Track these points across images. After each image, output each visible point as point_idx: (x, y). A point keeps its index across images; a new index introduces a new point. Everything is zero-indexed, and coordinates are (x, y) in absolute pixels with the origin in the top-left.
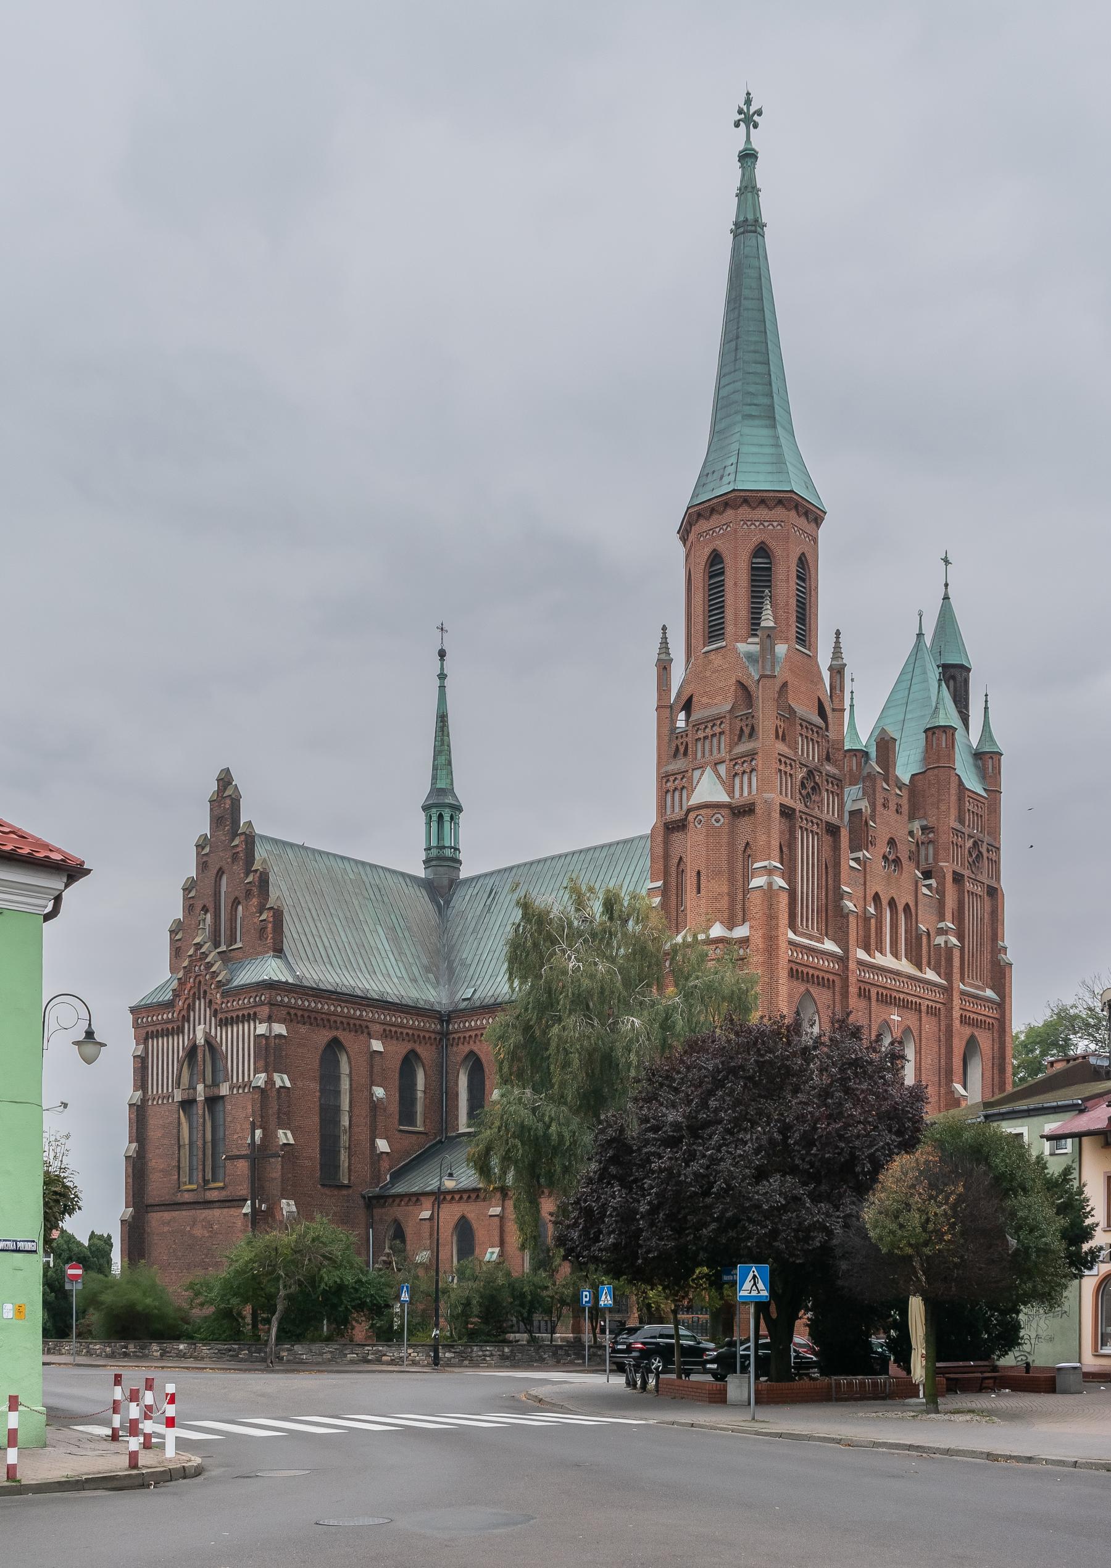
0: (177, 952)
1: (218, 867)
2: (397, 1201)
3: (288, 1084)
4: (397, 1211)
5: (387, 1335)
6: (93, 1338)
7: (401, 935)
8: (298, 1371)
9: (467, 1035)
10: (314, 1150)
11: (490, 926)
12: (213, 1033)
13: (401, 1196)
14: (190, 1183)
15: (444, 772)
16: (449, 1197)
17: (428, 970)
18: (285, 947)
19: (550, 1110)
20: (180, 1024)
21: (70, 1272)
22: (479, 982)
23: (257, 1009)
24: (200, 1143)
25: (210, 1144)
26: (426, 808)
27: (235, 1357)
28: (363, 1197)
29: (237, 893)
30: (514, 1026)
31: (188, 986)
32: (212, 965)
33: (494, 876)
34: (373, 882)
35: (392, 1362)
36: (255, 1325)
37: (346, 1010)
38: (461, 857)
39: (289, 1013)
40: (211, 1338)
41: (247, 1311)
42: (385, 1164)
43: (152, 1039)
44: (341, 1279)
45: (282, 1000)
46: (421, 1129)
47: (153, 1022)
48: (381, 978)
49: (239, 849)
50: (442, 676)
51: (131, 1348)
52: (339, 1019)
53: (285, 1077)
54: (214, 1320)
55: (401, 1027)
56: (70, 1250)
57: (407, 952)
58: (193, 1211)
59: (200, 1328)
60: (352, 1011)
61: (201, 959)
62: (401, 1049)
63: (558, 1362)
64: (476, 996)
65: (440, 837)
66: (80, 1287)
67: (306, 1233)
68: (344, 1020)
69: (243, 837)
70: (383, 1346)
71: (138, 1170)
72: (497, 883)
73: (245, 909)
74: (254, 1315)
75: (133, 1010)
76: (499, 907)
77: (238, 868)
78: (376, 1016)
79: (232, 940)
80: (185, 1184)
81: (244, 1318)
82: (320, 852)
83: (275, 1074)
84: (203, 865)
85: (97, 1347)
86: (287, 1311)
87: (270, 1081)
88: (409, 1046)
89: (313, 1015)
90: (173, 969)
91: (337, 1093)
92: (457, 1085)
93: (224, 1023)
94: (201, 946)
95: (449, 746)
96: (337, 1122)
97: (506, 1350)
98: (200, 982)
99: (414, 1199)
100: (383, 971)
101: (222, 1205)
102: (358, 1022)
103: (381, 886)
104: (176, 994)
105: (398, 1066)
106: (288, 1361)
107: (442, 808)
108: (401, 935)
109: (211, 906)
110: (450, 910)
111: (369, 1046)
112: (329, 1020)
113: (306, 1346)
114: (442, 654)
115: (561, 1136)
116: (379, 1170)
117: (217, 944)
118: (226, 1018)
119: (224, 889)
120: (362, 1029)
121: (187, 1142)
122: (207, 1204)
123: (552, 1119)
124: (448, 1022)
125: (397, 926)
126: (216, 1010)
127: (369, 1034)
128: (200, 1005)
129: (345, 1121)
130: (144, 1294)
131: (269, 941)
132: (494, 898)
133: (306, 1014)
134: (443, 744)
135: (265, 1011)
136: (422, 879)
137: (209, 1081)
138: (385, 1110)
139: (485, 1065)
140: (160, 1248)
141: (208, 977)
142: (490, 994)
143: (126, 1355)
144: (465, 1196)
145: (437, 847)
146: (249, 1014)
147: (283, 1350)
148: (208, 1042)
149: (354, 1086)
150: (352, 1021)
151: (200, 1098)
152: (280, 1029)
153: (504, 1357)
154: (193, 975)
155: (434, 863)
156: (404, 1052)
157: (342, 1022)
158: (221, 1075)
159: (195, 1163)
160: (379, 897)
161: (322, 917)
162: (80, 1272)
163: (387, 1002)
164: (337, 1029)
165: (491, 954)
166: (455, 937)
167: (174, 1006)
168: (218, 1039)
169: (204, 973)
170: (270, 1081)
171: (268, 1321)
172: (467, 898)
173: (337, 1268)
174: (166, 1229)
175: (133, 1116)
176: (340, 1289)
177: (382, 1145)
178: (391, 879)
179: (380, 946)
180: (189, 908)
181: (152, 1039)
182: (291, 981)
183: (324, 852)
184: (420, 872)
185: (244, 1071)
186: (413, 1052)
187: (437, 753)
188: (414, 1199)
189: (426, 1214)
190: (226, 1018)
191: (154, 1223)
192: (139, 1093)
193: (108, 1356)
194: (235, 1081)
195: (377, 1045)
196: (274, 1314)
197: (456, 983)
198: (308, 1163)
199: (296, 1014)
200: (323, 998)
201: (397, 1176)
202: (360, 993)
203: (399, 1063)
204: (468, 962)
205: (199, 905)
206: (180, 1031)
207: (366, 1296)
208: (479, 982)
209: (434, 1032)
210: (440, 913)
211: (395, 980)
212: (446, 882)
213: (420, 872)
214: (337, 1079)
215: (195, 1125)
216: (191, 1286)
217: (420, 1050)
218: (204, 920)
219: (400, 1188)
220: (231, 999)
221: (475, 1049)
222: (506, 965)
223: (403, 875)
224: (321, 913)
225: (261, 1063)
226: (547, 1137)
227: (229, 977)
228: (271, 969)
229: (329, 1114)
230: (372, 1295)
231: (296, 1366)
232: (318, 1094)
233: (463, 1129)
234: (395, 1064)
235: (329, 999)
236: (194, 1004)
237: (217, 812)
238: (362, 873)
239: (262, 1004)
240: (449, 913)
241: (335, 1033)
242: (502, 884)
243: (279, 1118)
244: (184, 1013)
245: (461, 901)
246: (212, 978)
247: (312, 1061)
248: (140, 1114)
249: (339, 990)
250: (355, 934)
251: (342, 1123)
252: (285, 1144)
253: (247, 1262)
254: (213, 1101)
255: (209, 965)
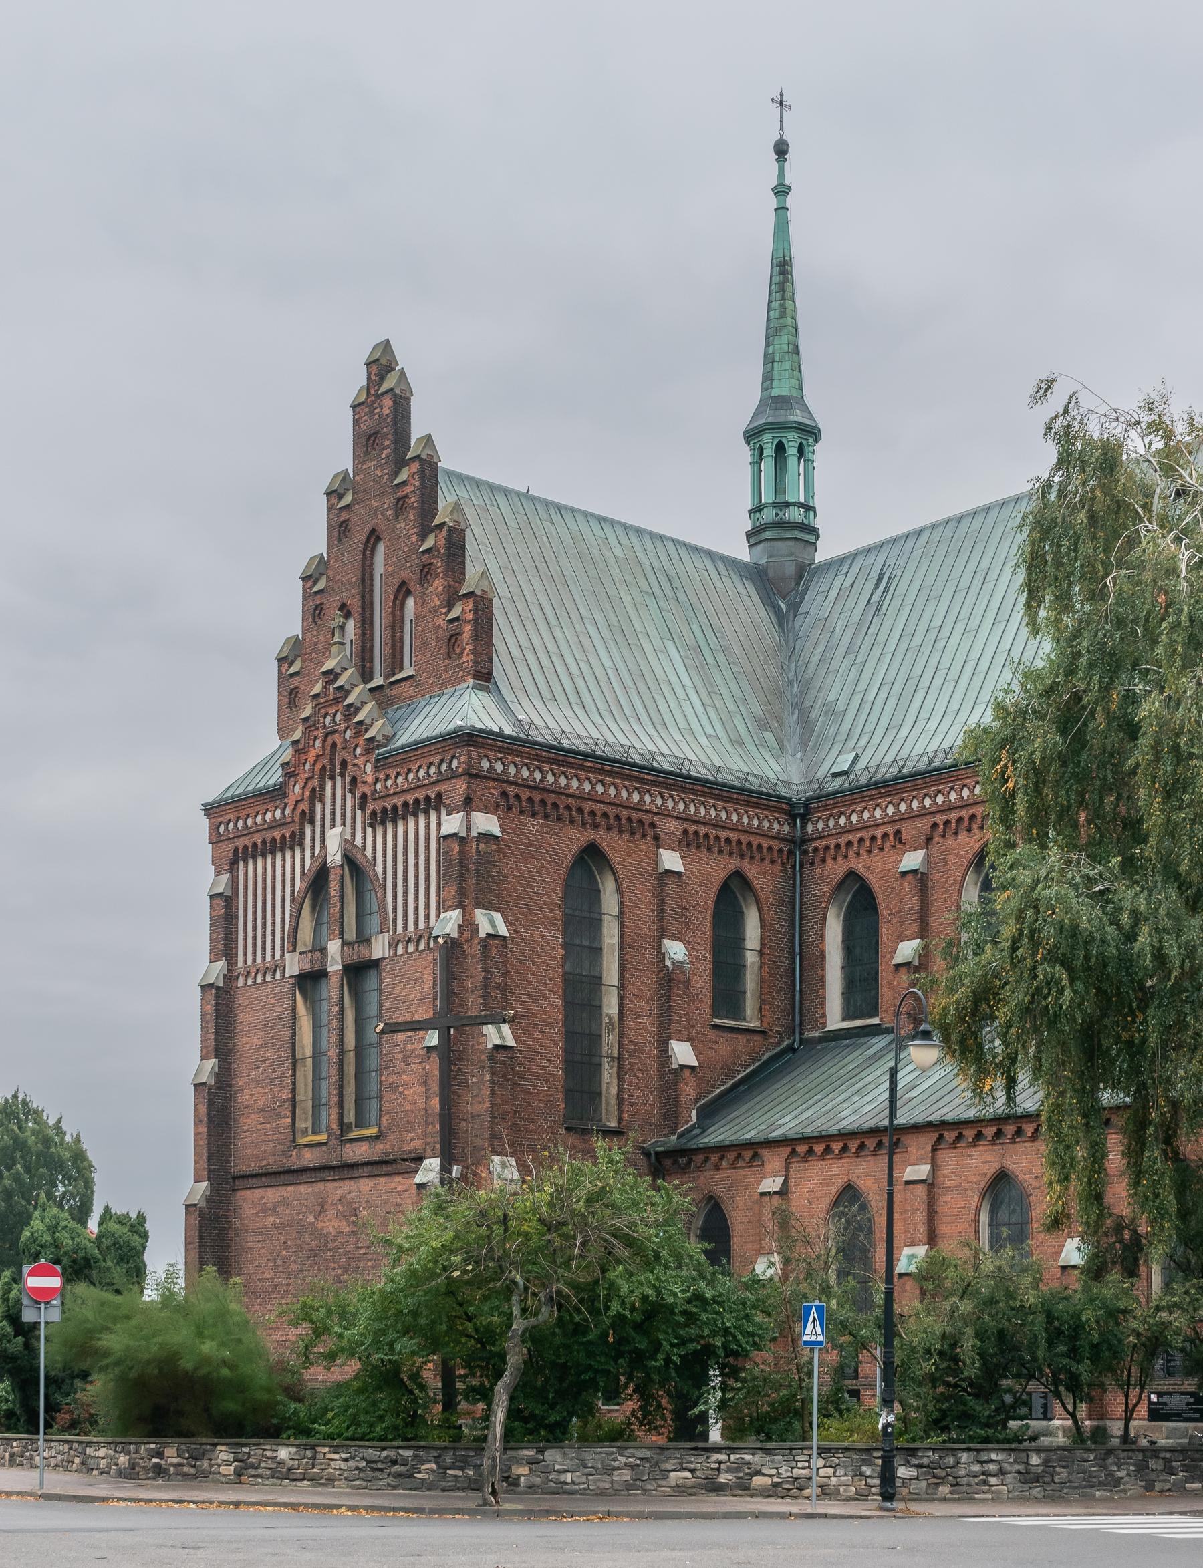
0: (290, 696)
1: (367, 529)
2: (714, 1158)
3: (503, 930)
4: (716, 1180)
5: (774, 1422)
6: (102, 1433)
7: (710, 660)
8: (559, 1514)
9: (843, 841)
10: (550, 1063)
11: (882, 638)
12: (358, 841)
13: (721, 1149)
14: (314, 1132)
15: (787, 366)
16: (819, 1148)
17: (763, 725)
18: (497, 673)
19: (1131, 897)
20: (296, 828)
21: (34, 1282)
22: (863, 742)
23: (441, 788)
24: (333, 1053)
25: (352, 1054)
26: (752, 435)
27: (406, 1478)
28: (647, 1154)
29: (403, 574)
30: (1041, 716)
31: (312, 755)
32: (357, 710)
33: (885, 549)
34: (656, 564)
35: (775, 1491)
36: (449, 1405)
37: (612, 791)
38: (818, 523)
39: (504, 794)
40: (353, 1433)
41: (431, 1375)
42: (688, 1090)
43: (245, 861)
44: (659, 1293)
45: (491, 768)
46: (755, 1024)
47: (246, 828)
48: (678, 737)
49: (408, 490)
50: (782, 190)
51: (171, 1455)
52: (600, 809)
53: (497, 916)
54: (361, 1391)
55: (716, 826)
56: (57, 1245)
57: (724, 691)
58: (321, 1185)
59: (326, 1410)
60: (624, 794)
61: (336, 701)
62: (719, 868)
63: (1149, 1487)
64: (861, 765)
65: (779, 487)
66: (55, 1316)
67: (575, 1182)
68: (611, 811)
69: (415, 466)
70: (753, 1451)
71: (218, 1107)
72: (891, 561)
73: (421, 601)
74: (448, 1376)
75: (210, 810)
76: (896, 602)
77: (407, 526)
78: (670, 804)
79: (395, 663)
80: (305, 1132)
81: (423, 1387)
82: (559, 508)
83: (477, 910)
84: (339, 529)
85: (102, 1452)
86: (530, 1366)
87: (468, 925)
88: (732, 864)
89: (550, 799)
90: (283, 731)
91: (596, 952)
92: (822, 938)
93: (379, 820)
94: (337, 676)
95: (794, 318)
96: (596, 1009)
97: (1035, 1460)
98: (334, 745)
99: (747, 1154)
100: (689, 724)
101: (374, 1170)
102: (635, 815)
103: (672, 572)
104: (290, 771)
105: (711, 904)
106: (531, 1488)
107: (782, 434)
108: (710, 660)
109: (355, 604)
110: (799, 619)
111: (656, 861)
112: (580, 810)
113: (572, 1453)
114: (781, 150)
115: (1160, 957)
116: (677, 1102)
117: (366, 676)
118: (384, 810)
119: (379, 568)
120: (642, 828)
121: (309, 1052)
122: (348, 1169)
123: (1135, 914)
124: (805, 819)
125: (703, 644)
126: (364, 797)
127: (656, 838)
128: (335, 789)
129: (611, 1006)
130: (200, 1334)
131: (467, 658)
132: (886, 589)
133: (537, 797)
134: (783, 315)
135: (459, 788)
136: (745, 564)
137: (350, 935)
138: (687, 983)
139: (879, 897)
140: (259, 1257)
141: (348, 734)
142: (889, 758)
143: (159, 1471)
144: (854, 1145)
145: (775, 505)
146: (428, 799)
147: (518, 1462)
148: (348, 859)
149: (628, 939)
150: (624, 813)
151: (335, 967)
152: (486, 823)
153: (1028, 1478)
154: (321, 733)
155: (768, 534)
156: (722, 874)
157: (605, 815)
158: (374, 922)
159: (324, 1093)
160: (669, 593)
161: (565, 621)
162: (55, 1282)
163: (690, 777)
164: (596, 827)
165: (885, 689)
166: (812, 666)
167: (284, 796)
168: (369, 852)
169: (341, 727)
170: (468, 925)
171: (485, 1395)
172: (833, 594)
173: (649, 1266)
174: (270, 1220)
175: (210, 1009)
176: (654, 1312)
177: (683, 1053)
178: (690, 564)
179: (674, 679)
180: (315, 612)
181: (245, 861)
182: (508, 731)
183: (566, 508)
184: (742, 553)
185: (419, 910)
186: (738, 875)
187: (773, 331)
188: (747, 1154)
189: (772, 1184)
190: (384, 810)
191: (248, 1211)
192: (221, 965)
193: (121, 1474)
194: (400, 929)
195: (671, 860)
196: (499, 1375)
197: (816, 748)
198: (540, 1086)
199: (517, 797)
200: (569, 765)
201: (711, 1112)
202: (639, 760)
203: (713, 895)
204: (841, 706)
205: (333, 602)
206: (296, 841)
207: (714, 1334)
208: (863, 742)
209: (777, 838)
210: (781, 624)
211: (704, 740)
212: (790, 570)
213: (742, 553)
214: (594, 924)
215: (324, 1019)
216: (306, 1313)
217: (752, 872)
218: (342, 628)
219: (720, 1134)
220: (393, 772)
221: (859, 867)
222: (1021, 576)
223: (711, 555)
224: (562, 613)
225: (451, 891)
226: (1126, 962)
227: (388, 731)
228: (471, 709)
229: (581, 993)
230: (727, 1330)
231: (551, 1501)
232: (560, 952)
233: (835, 1020)
234: (704, 897)
235: (581, 767)
236: (323, 788)
237: (367, 425)
238: (638, 548)
239: (453, 775)
240: (798, 623)
241: (593, 835)
242: (902, 561)
243: (485, 996)
244: (305, 806)
245: (818, 602)
246: (357, 734)
247: (549, 886)
248: (221, 1002)
249: (599, 752)
250: (625, 652)
251: (606, 1010)
252: (497, 1047)
253: (437, 1254)
254: (359, 972)
255: (352, 710)
